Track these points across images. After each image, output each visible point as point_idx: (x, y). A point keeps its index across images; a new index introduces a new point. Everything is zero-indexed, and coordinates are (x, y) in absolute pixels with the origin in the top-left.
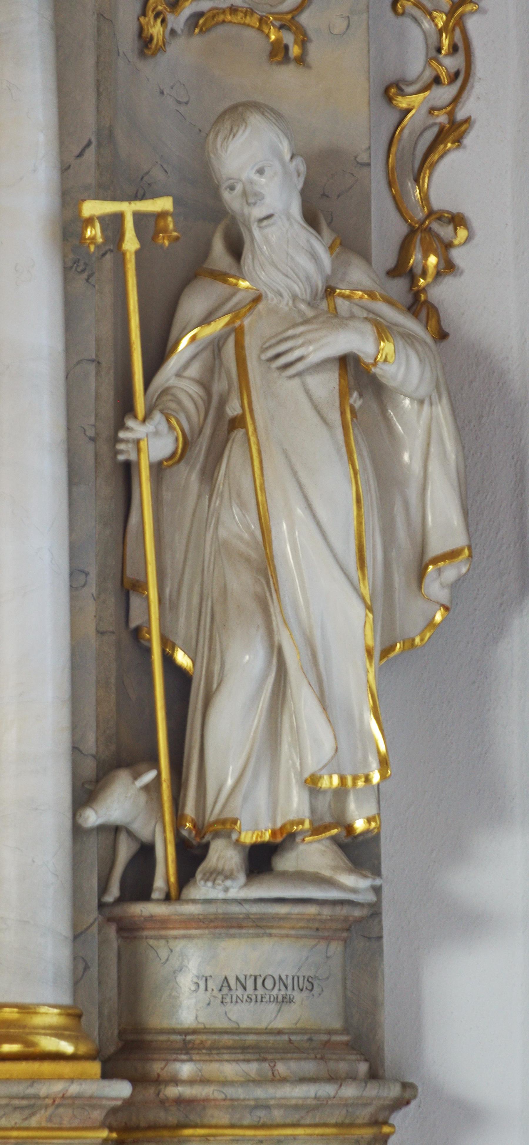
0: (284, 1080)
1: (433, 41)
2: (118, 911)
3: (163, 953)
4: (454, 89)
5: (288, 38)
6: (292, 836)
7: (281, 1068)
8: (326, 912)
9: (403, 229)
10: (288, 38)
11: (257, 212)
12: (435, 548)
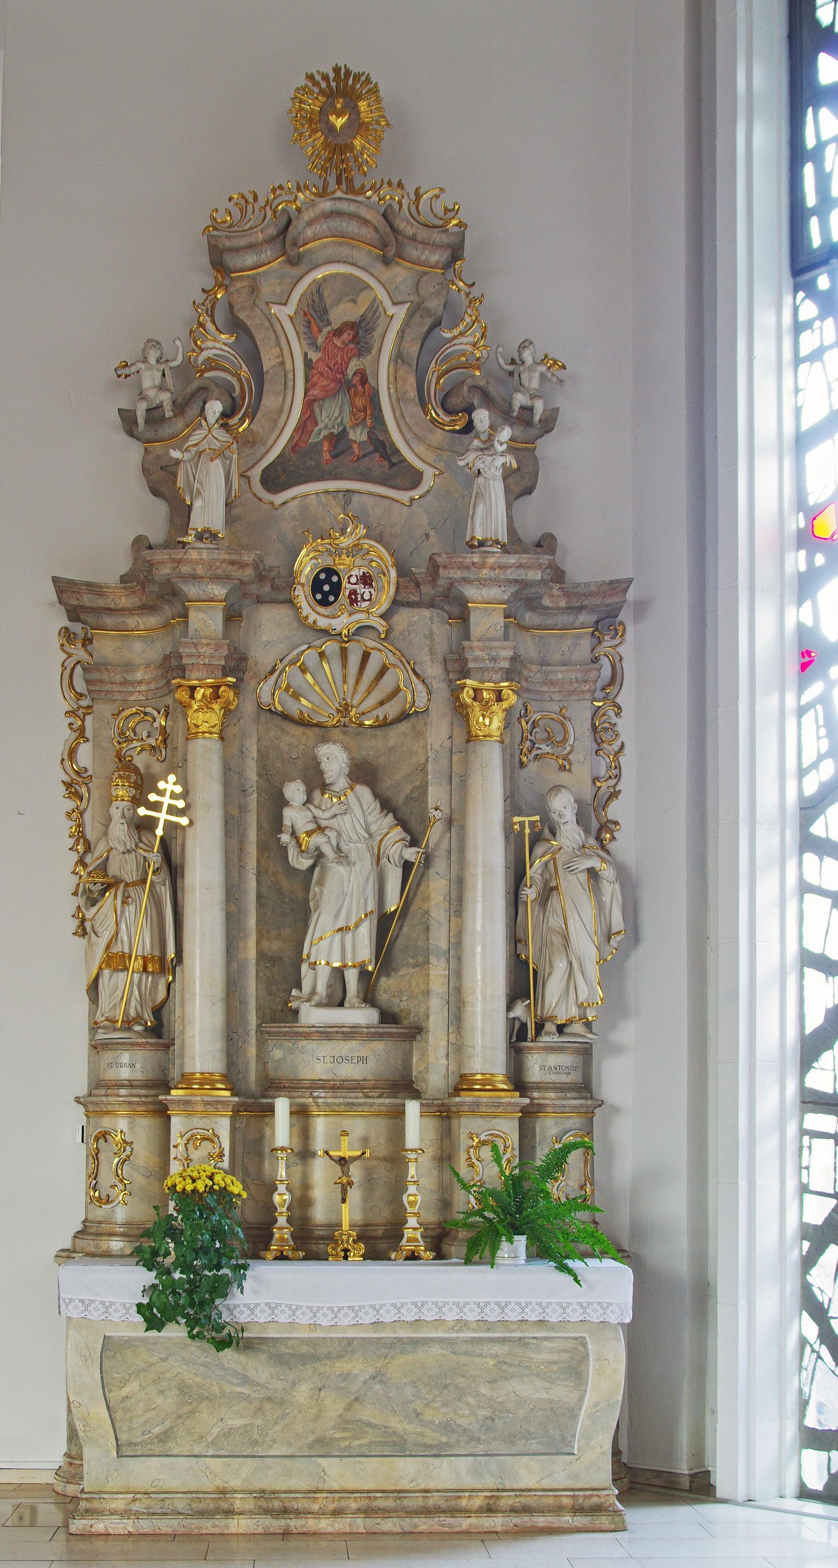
0: (569, 1098)
1: (609, 765)
2: (516, 1044)
3: (530, 1058)
4: (616, 780)
5: (566, 763)
6: (572, 1022)
7: (568, 1095)
8: (581, 1045)
9: (599, 826)
10: (566, 763)
11: (563, 821)
12: (614, 930)
